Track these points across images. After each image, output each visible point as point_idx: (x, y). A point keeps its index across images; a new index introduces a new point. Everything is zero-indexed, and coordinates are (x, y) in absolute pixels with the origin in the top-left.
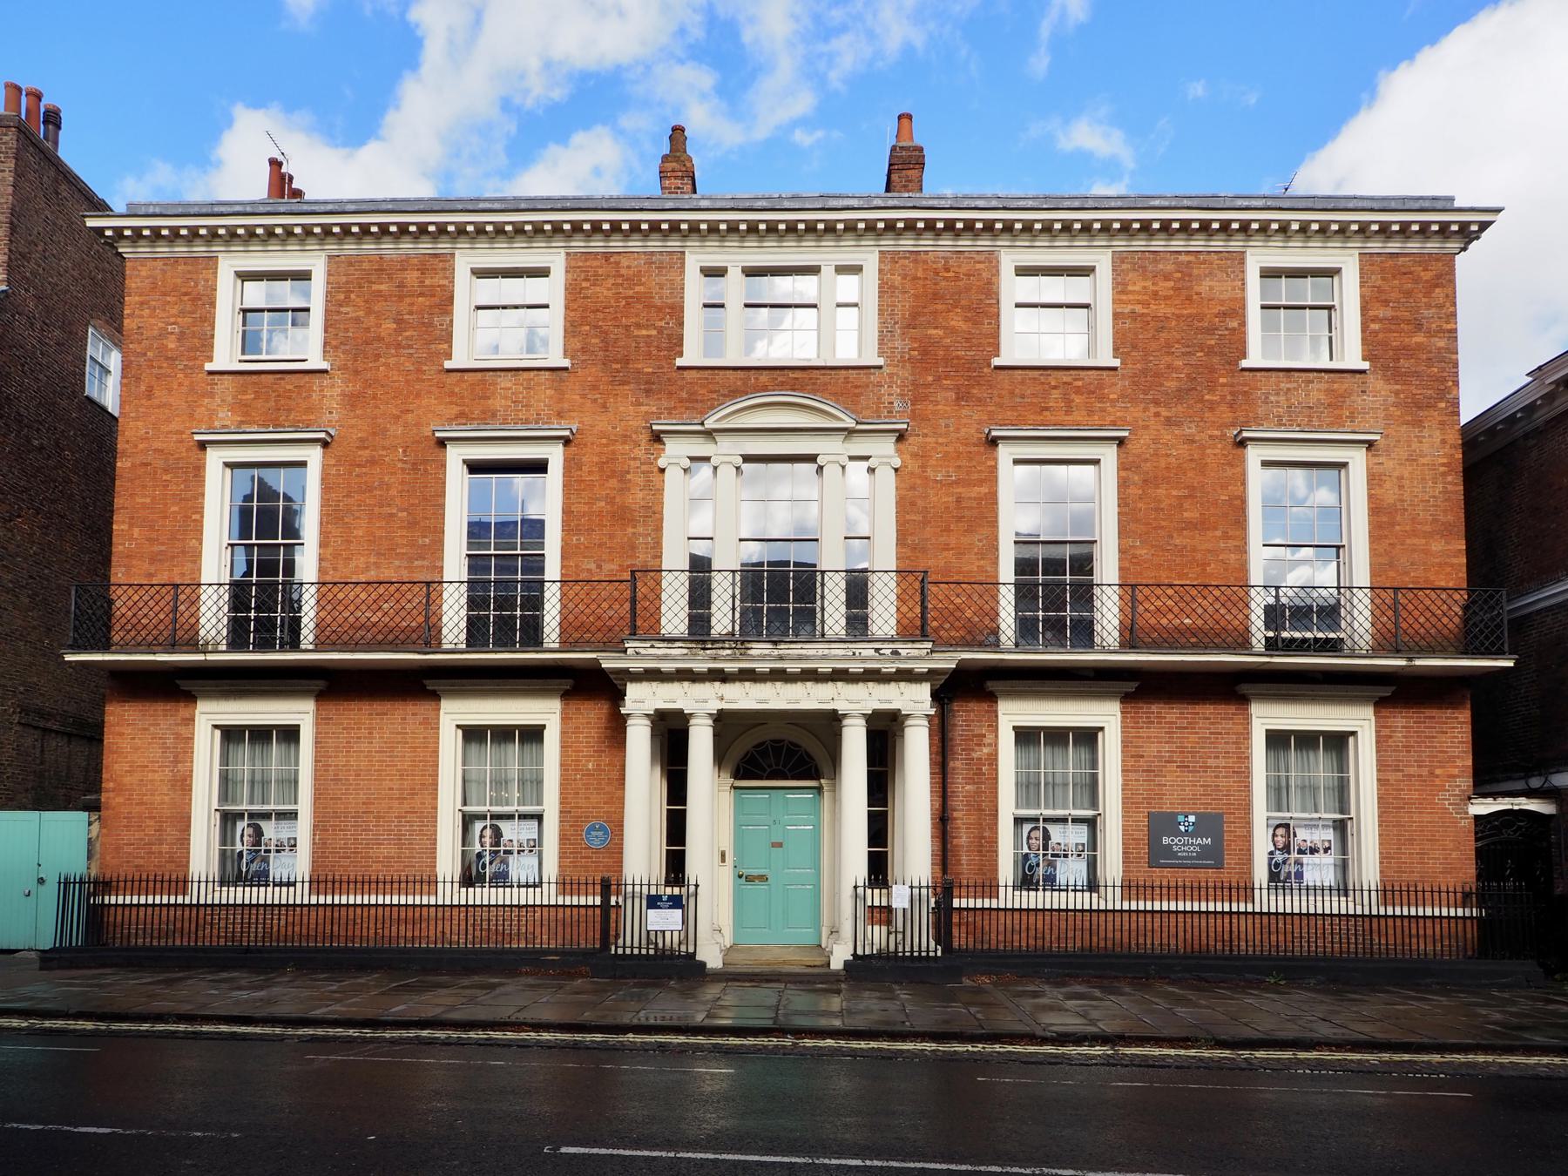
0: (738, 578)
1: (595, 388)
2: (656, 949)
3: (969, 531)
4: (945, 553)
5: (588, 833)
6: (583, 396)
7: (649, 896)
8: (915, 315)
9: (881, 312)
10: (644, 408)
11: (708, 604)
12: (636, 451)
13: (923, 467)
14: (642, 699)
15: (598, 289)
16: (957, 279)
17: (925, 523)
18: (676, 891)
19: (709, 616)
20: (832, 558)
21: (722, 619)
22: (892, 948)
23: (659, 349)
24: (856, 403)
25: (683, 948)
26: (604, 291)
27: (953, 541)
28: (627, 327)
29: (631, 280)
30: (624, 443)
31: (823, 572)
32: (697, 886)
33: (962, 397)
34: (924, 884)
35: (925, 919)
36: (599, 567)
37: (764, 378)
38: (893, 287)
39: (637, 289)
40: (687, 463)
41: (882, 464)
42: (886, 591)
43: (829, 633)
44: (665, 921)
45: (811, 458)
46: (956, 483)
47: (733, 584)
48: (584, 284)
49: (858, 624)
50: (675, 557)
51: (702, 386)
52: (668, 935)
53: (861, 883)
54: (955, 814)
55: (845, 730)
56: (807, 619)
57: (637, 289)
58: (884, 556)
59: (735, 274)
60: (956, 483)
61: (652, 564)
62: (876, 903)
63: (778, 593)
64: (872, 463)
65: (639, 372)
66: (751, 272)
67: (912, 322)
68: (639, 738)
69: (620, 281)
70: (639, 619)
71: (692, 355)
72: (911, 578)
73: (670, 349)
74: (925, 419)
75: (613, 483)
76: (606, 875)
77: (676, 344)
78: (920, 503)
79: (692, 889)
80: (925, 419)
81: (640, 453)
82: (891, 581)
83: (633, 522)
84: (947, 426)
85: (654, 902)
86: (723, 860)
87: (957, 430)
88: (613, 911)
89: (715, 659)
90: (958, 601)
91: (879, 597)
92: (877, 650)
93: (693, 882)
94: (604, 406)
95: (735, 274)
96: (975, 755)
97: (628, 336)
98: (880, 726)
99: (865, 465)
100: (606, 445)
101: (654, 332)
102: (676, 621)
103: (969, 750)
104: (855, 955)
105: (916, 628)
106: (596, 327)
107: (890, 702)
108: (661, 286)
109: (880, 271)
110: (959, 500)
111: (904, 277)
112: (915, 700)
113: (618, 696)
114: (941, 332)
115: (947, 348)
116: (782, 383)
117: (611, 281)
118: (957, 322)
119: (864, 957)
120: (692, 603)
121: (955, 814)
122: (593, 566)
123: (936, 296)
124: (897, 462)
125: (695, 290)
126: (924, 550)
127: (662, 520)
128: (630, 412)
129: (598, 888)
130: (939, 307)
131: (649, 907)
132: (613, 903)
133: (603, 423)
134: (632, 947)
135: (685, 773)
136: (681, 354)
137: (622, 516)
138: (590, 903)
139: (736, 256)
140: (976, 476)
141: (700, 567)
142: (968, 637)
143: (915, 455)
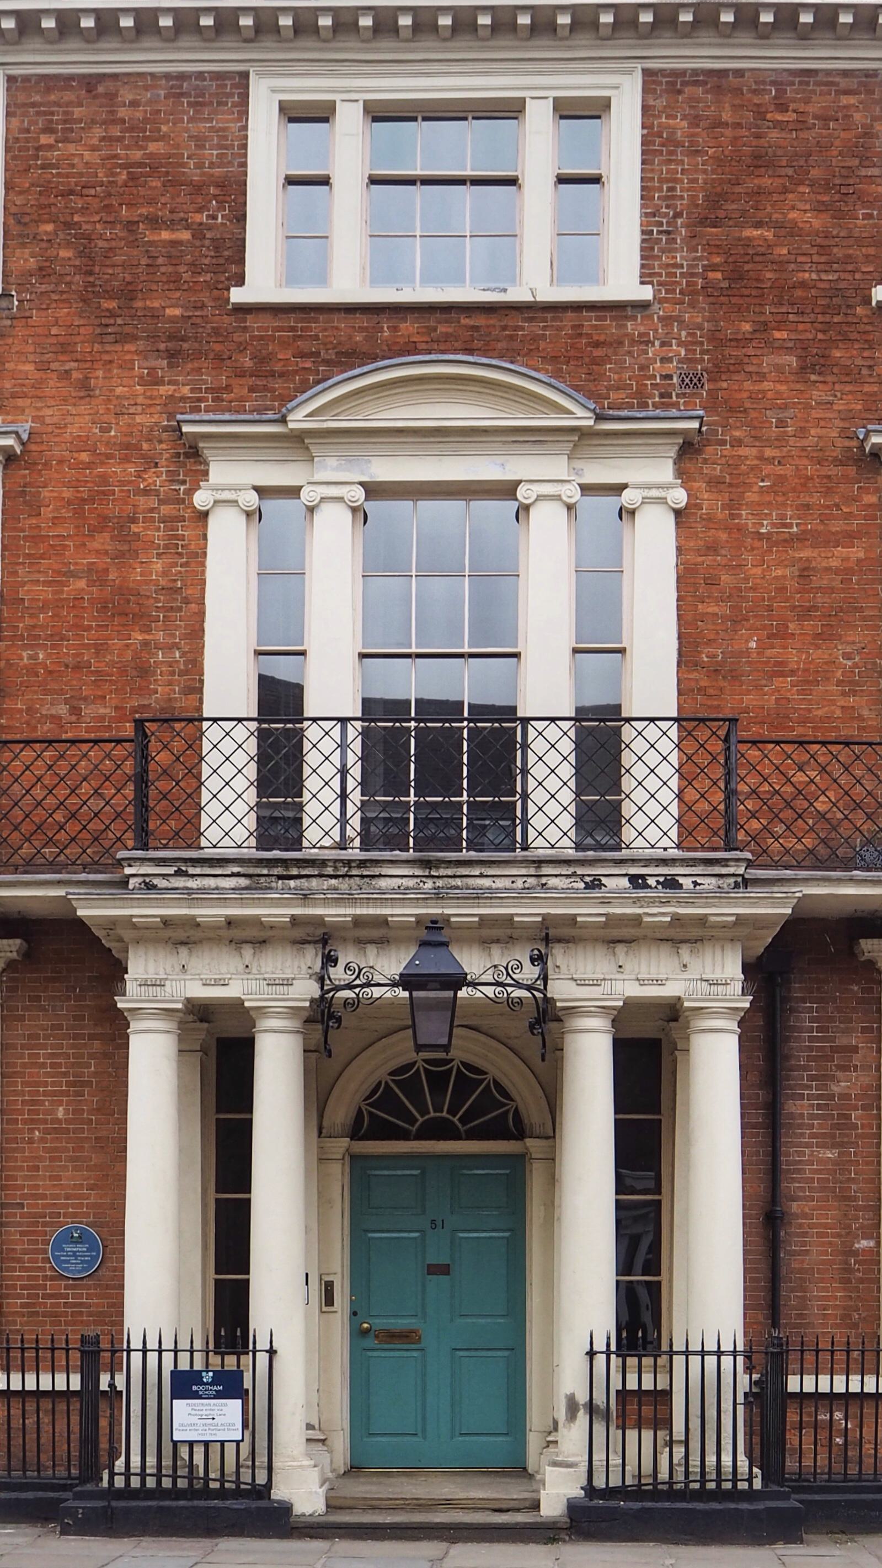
0: (351, 733)
1: (65, 348)
2: (191, 1477)
3: (824, 637)
4: (778, 682)
5: (58, 1246)
6: (43, 367)
7: (175, 1374)
8: (716, 199)
9: (646, 193)
10: (165, 390)
11: (295, 785)
12: (150, 476)
13: (733, 506)
14: (157, 983)
15: (72, 148)
16: (801, 125)
17: (737, 620)
18: (231, 1361)
19: (300, 807)
20: (546, 688)
21: (328, 809)
22: (664, 1475)
23: (196, 268)
24: (594, 377)
25: (246, 1476)
26: (83, 155)
27: (794, 658)
28: (131, 226)
29: (139, 132)
30: (126, 459)
31: (526, 721)
32: (272, 1352)
33: (813, 364)
34: (727, 1346)
35: (733, 1423)
36: (75, 711)
37: (409, 327)
38: (672, 142)
39: (152, 147)
40: (251, 499)
41: (645, 501)
42: (652, 758)
43: (539, 847)
44: (206, 1421)
45: (507, 490)
46: (801, 539)
47: (343, 746)
48: (45, 139)
49: (600, 817)
50: (228, 687)
51: (284, 344)
52: (215, 1450)
53: (600, 1345)
54: (795, 1207)
55: (569, 1038)
56: (499, 820)
57: (152, 147)
58: (651, 684)
59: (349, 117)
60: (801, 539)
61: (183, 703)
62: (632, 1385)
63: (439, 774)
64: (628, 497)
65: (155, 315)
66: (379, 114)
67: (710, 213)
68: (154, 1072)
69: (116, 132)
70: (157, 806)
71: (262, 282)
72: (702, 733)
73: (217, 269)
74: (735, 409)
75: (102, 541)
76: (91, 1332)
77: (230, 259)
78: (726, 578)
79: (262, 1359)
80: (735, 409)
81: (157, 479)
82: (666, 741)
83: (142, 619)
84: (781, 423)
85: (185, 1385)
86: (329, 1299)
87: (802, 432)
88: (103, 1406)
89: (306, 898)
90: (800, 778)
91: (639, 771)
92: (633, 879)
93: (263, 1344)
94: (84, 385)
95: (349, 117)
96: (835, 1089)
97: (134, 244)
98: (644, 1029)
99: (610, 503)
100: (90, 465)
101: (185, 235)
102: (227, 746)
103: (824, 1079)
104: (590, 1490)
105: (714, 826)
106: (68, 225)
107: (659, 982)
108: (200, 141)
109: (646, 109)
110: (805, 573)
111: (695, 121)
112: (712, 983)
113: (115, 972)
114: (769, 234)
115: (781, 265)
116: (447, 337)
117: (98, 132)
118: (804, 216)
119: (609, 1493)
120: (264, 785)
121: (795, 1207)
122: (62, 710)
123: (760, 162)
124: (679, 497)
125: (267, 149)
126: (734, 676)
127: (201, 614)
128: (132, 392)
129: (75, 1356)
130: (766, 182)
131: (176, 1395)
132: (104, 1386)
133: (80, 421)
134: (143, 1475)
135: (247, 1127)
136: (240, 280)
137: (124, 608)
138: (61, 1385)
139: (350, 88)
140: (837, 526)
141: (280, 703)
142: (822, 851)
143: (715, 483)
